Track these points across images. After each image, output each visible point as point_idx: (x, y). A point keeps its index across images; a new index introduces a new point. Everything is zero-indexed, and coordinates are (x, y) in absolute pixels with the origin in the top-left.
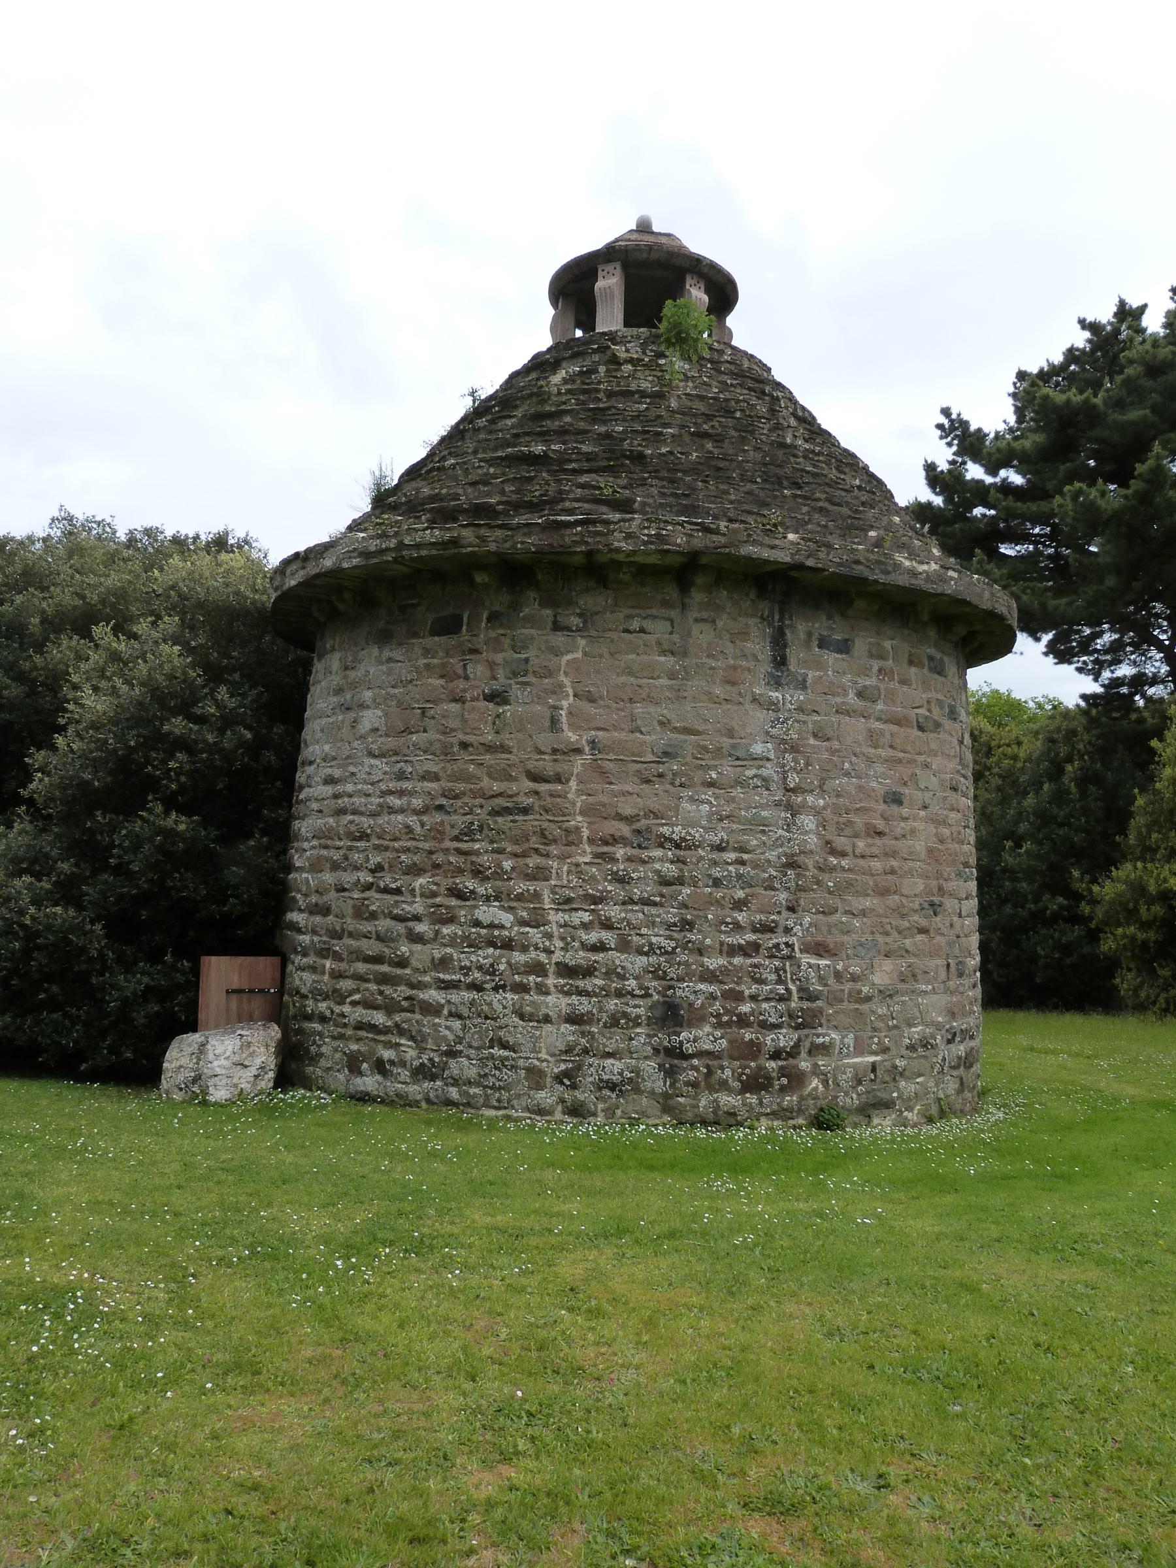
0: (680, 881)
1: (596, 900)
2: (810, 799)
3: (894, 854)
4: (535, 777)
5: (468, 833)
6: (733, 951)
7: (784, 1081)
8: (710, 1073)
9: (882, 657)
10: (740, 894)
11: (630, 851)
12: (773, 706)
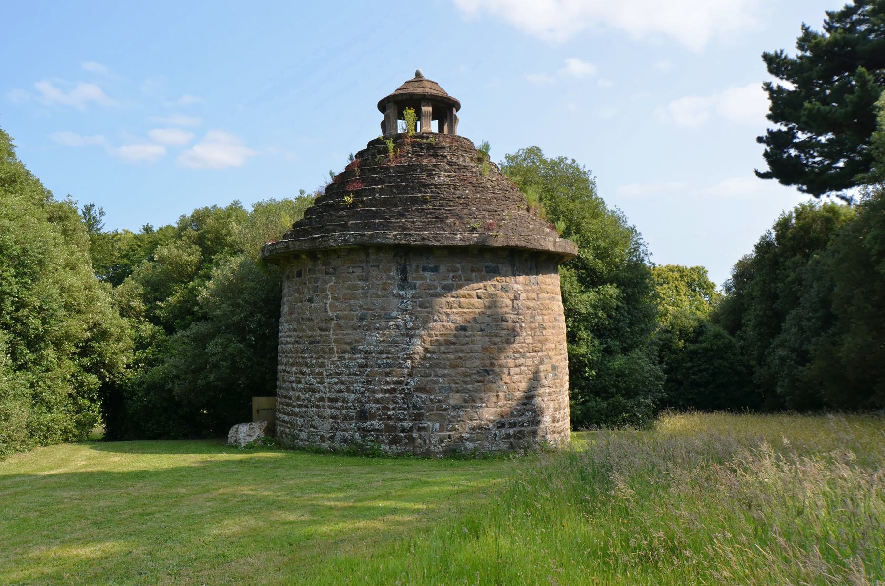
0: (367, 366)
1: (339, 374)
2: (417, 332)
3: (461, 351)
4: (321, 330)
5: (303, 351)
6: (386, 391)
7: (407, 441)
8: (377, 437)
9: (454, 271)
10: (388, 370)
11: (349, 356)
12: (401, 297)
